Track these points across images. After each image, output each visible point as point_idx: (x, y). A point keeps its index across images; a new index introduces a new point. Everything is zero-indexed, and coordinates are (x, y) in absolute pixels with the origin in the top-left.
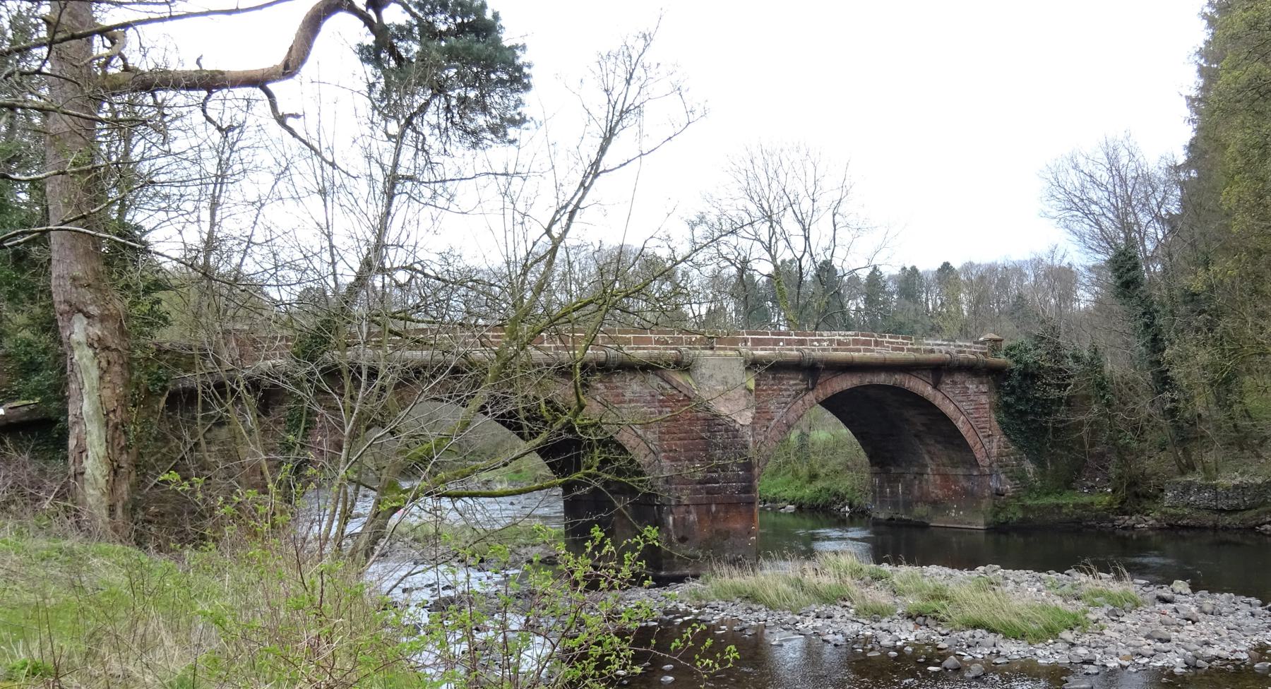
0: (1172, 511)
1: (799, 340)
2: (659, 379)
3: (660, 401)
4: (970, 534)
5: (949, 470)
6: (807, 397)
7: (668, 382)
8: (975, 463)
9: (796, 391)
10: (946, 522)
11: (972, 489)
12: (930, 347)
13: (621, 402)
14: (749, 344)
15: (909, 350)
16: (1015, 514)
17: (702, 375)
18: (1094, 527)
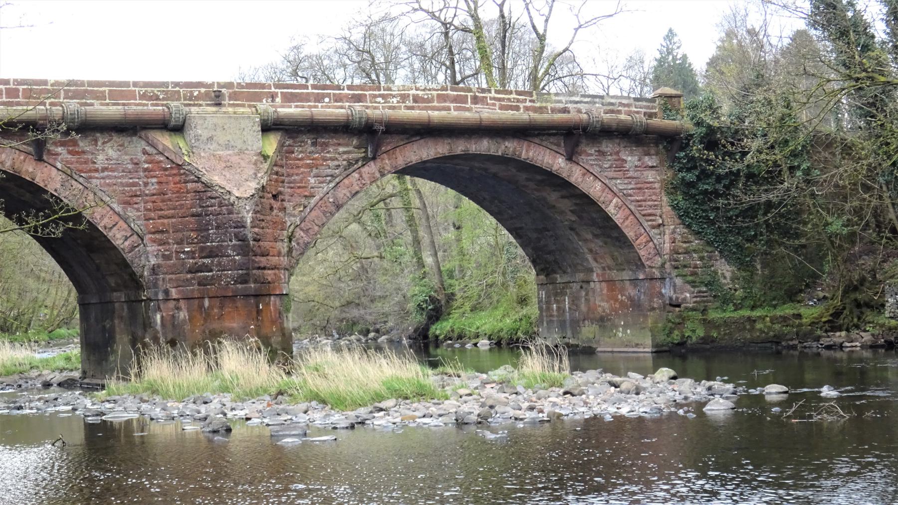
1: (354, 96)
2: (143, 143)
3: (145, 170)
4: (638, 359)
5: (614, 274)
6: (366, 169)
7: (153, 146)
8: (639, 264)
9: (348, 161)
10: (614, 345)
11: (639, 298)
12: (561, 106)
13: (90, 171)
14: (278, 100)
15: (527, 109)
16: (694, 331)
17: (197, 138)
18: (794, 347)
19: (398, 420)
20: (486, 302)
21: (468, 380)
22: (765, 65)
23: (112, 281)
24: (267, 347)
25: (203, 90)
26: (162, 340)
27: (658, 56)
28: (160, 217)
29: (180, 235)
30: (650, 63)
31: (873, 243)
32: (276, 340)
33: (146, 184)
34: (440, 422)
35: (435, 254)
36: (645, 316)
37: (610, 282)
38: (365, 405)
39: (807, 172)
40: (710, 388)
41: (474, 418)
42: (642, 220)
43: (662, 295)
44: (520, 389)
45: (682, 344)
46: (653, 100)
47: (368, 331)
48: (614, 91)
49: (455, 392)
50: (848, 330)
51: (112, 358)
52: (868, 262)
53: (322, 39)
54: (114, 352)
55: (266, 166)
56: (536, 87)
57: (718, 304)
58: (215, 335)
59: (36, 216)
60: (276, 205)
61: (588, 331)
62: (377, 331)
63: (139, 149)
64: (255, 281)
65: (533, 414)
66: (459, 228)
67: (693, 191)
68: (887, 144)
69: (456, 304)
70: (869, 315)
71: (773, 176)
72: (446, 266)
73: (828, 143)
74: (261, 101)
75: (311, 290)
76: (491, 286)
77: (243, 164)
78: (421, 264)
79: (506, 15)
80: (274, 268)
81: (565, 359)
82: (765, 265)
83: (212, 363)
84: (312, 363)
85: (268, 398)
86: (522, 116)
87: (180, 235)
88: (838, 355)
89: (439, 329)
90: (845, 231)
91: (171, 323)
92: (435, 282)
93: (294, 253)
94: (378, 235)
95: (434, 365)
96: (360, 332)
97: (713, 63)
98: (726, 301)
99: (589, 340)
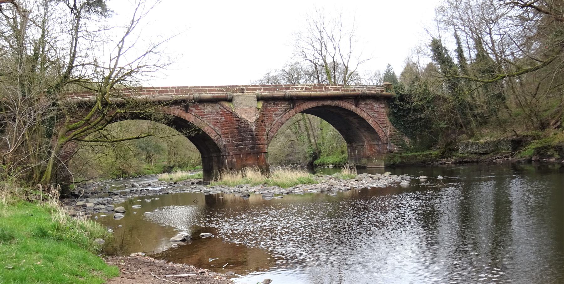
0: (461, 155)
1: (286, 88)
3: (220, 114)
5: (372, 143)
6: (291, 112)
7: (222, 106)
8: (379, 139)
9: (285, 109)
12: (353, 89)
14: (262, 90)
15: (342, 90)
17: (237, 103)
18: (430, 164)
19: (302, 191)
20: (331, 153)
21: (325, 177)
22: (419, 74)
23: (211, 150)
24: (261, 169)
25: (238, 88)
26: (228, 168)
27: (385, 73)
28: (226, 129)
29: (232, 135)
30: (382, 75)
31: (454, 130)
32: (264, 167)
33: (221, 119)
34: (316, 191)
35: (315, 139)
36: (382, 156)
37: (370, 145)
38: (292, 186)
39: (433, 108)
40: (402, 178)
41: (326, 189)
42: (380, 125)
43: (387, 149)
44: (341, 180)
45: (394, 164)
46: (382, 86)
47: (294, 164)
48: (371, 84)
49: (320, 181)
50: (447, 158)
51: (212, 175)
52: (453, 136)
53: (276, 70)
54: (213, 172)
55: (259, 111)
56: (345, 83)
57: (405, 151)
58: (244, 166)
59: (186, 130)
60: (263, 124)
61: (364, 161)
62: (297, 163)
63: (218, 108)
64: (257, 149)
65: (345, 187)
66: (322, 130)
67: (396, 115)
68: (458, 98)
69: (321, 154)
70: (454, 153)
71: (422, 109)
72: (318, 142)
73: (437, 98)
74: (256, 91)
75: (276, 151)
76: (333, 148)
77: (251, 111)
78: (310, 141)
79: (335, 60)
80: (263, 144)
81: (356, 170)
82: (420, 138)
83: (244, 175)
84: (275, 173)
85: (261, 185)
86: (340, 93)
87: (232, 135)
88: (444, 166)
89: (317, 162)
90: (445, 126)
91: (231, 163)
92: (315, 147)
93: (269, 139)
94: (296, 133)
95: (314, 173)
96: (292, 164)
97: (402, 74)
98: (408, 150)
99: (364, 164)
